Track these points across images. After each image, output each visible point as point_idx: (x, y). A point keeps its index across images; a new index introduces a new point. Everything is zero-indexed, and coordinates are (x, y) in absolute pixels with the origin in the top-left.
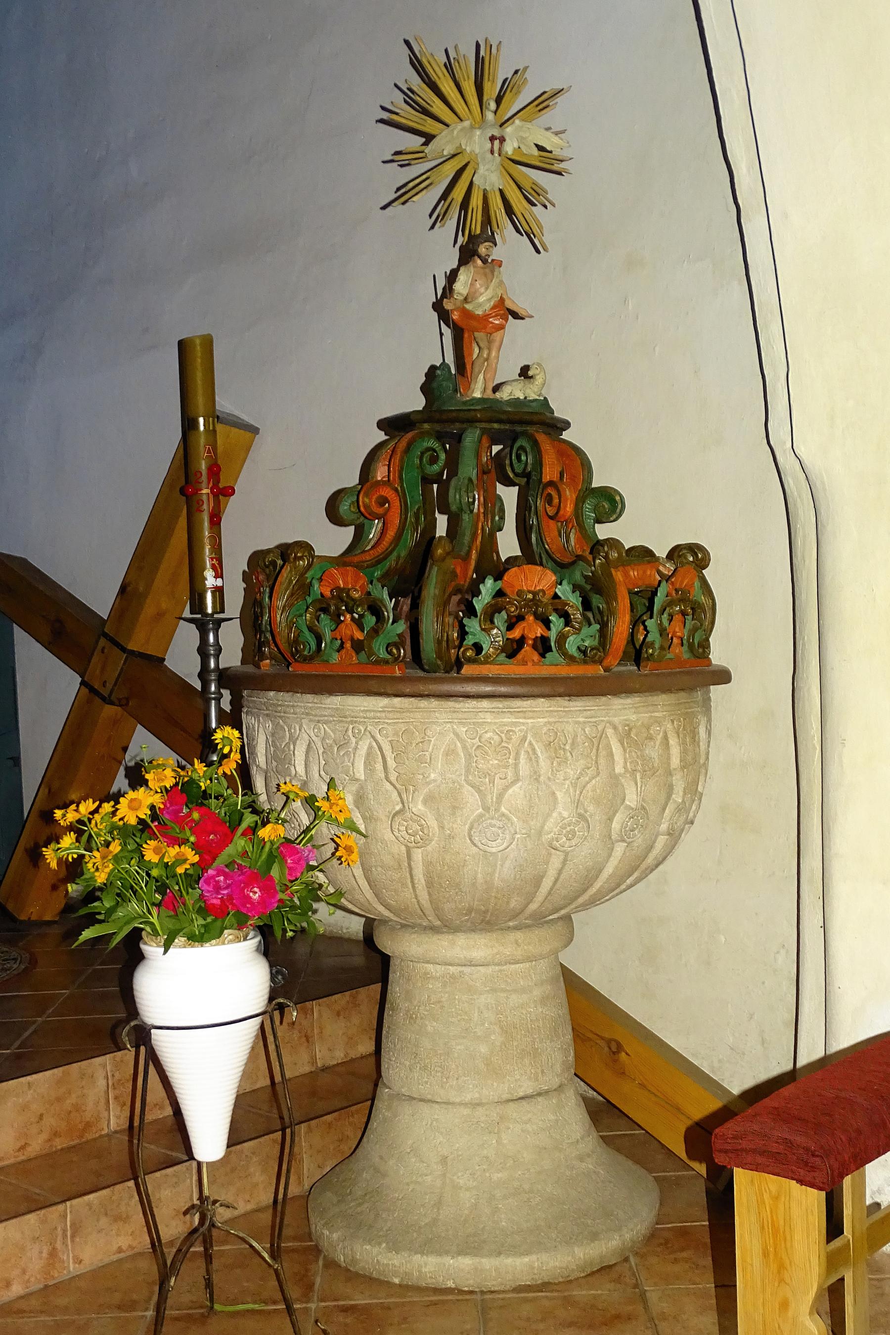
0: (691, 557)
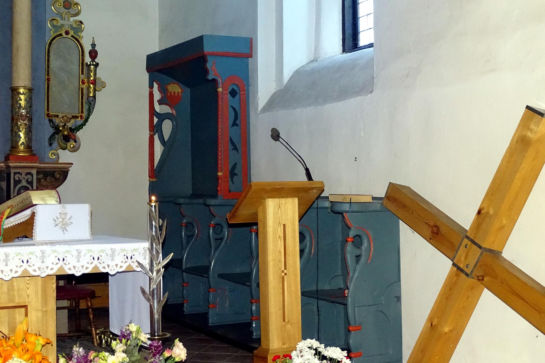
0: (392, 186)
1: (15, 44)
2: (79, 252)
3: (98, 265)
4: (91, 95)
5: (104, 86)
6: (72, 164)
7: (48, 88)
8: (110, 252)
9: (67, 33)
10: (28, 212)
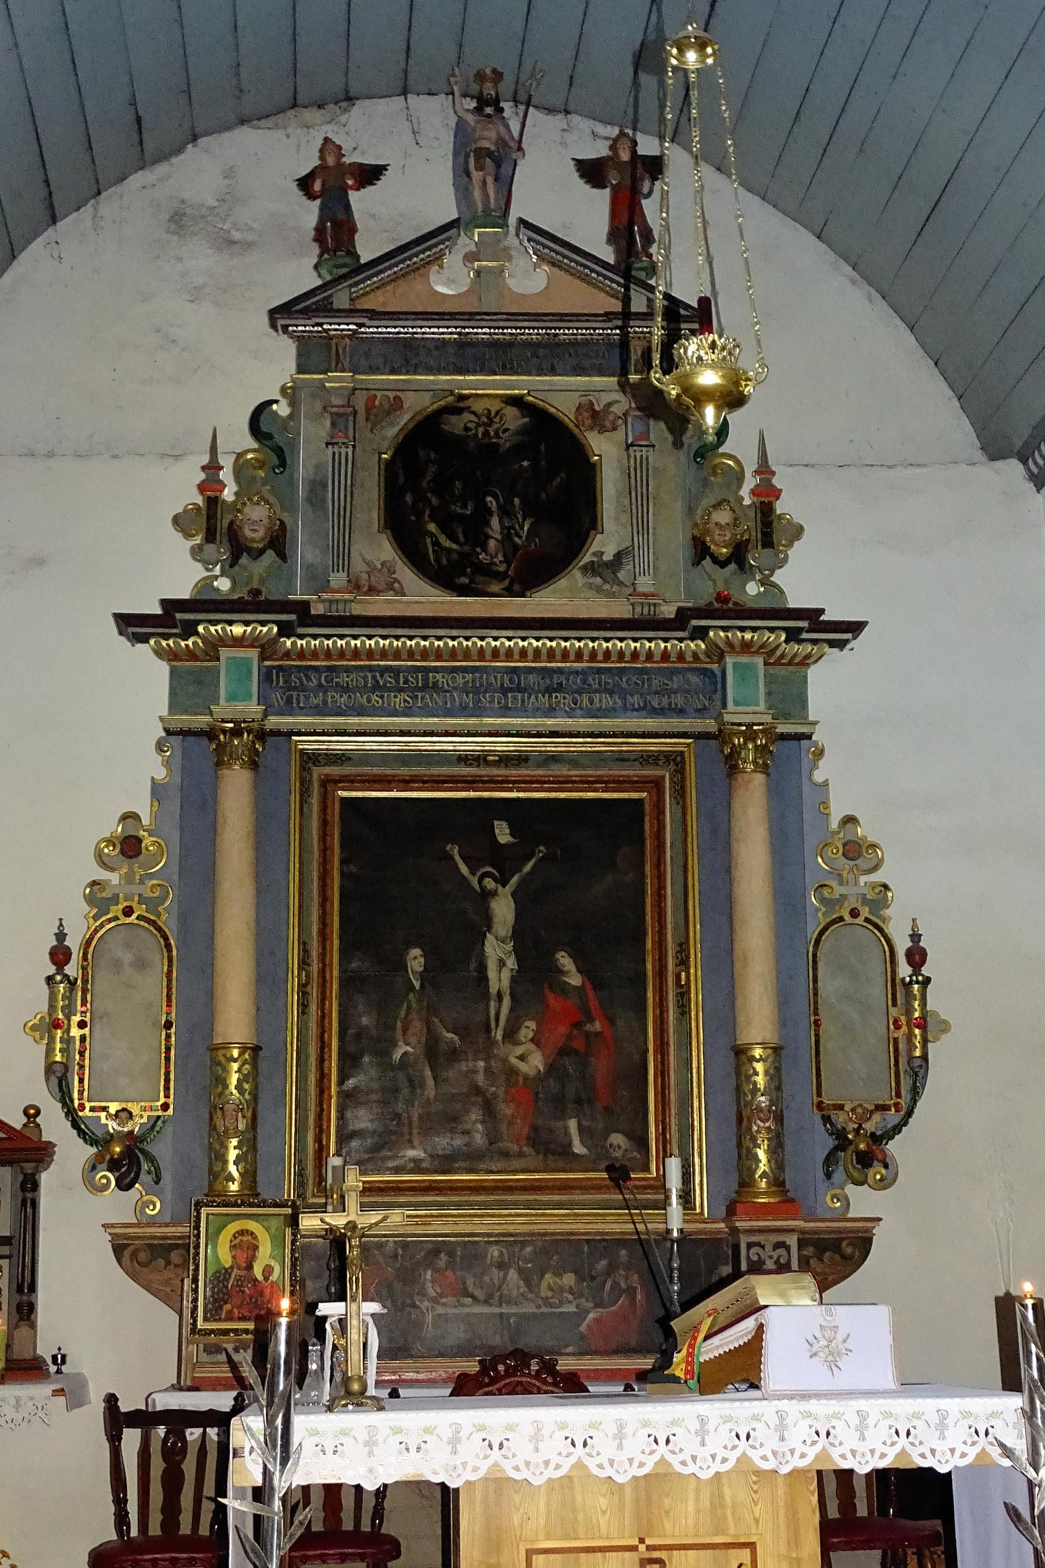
1: (738, 953)
2: (862, 1415)
3: (909, 1449)
4: (918, 1053)
5: (945, 1027)
6: (880, 1219)
7: (817, 1042)
8: (934, 1419)
9: (854, 913)
10: (749, 1324)
